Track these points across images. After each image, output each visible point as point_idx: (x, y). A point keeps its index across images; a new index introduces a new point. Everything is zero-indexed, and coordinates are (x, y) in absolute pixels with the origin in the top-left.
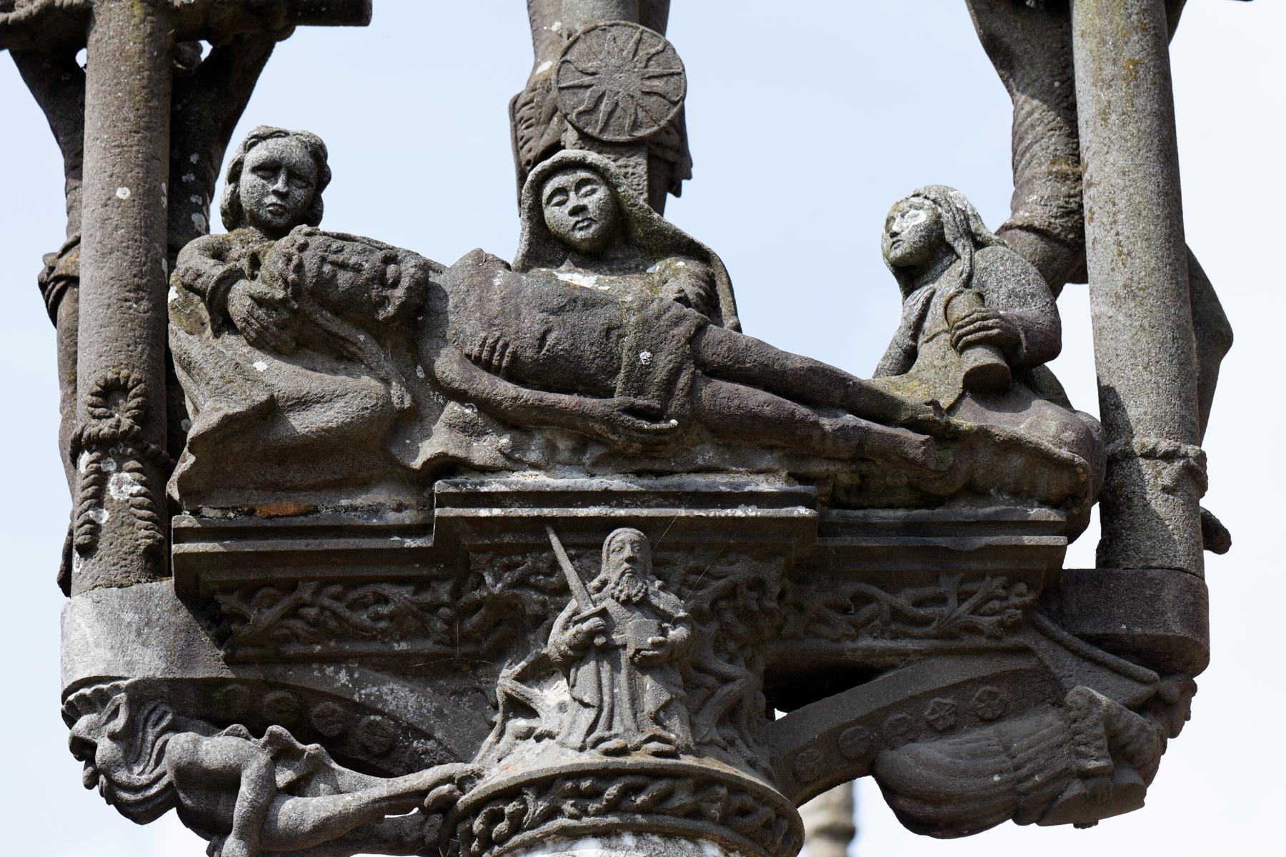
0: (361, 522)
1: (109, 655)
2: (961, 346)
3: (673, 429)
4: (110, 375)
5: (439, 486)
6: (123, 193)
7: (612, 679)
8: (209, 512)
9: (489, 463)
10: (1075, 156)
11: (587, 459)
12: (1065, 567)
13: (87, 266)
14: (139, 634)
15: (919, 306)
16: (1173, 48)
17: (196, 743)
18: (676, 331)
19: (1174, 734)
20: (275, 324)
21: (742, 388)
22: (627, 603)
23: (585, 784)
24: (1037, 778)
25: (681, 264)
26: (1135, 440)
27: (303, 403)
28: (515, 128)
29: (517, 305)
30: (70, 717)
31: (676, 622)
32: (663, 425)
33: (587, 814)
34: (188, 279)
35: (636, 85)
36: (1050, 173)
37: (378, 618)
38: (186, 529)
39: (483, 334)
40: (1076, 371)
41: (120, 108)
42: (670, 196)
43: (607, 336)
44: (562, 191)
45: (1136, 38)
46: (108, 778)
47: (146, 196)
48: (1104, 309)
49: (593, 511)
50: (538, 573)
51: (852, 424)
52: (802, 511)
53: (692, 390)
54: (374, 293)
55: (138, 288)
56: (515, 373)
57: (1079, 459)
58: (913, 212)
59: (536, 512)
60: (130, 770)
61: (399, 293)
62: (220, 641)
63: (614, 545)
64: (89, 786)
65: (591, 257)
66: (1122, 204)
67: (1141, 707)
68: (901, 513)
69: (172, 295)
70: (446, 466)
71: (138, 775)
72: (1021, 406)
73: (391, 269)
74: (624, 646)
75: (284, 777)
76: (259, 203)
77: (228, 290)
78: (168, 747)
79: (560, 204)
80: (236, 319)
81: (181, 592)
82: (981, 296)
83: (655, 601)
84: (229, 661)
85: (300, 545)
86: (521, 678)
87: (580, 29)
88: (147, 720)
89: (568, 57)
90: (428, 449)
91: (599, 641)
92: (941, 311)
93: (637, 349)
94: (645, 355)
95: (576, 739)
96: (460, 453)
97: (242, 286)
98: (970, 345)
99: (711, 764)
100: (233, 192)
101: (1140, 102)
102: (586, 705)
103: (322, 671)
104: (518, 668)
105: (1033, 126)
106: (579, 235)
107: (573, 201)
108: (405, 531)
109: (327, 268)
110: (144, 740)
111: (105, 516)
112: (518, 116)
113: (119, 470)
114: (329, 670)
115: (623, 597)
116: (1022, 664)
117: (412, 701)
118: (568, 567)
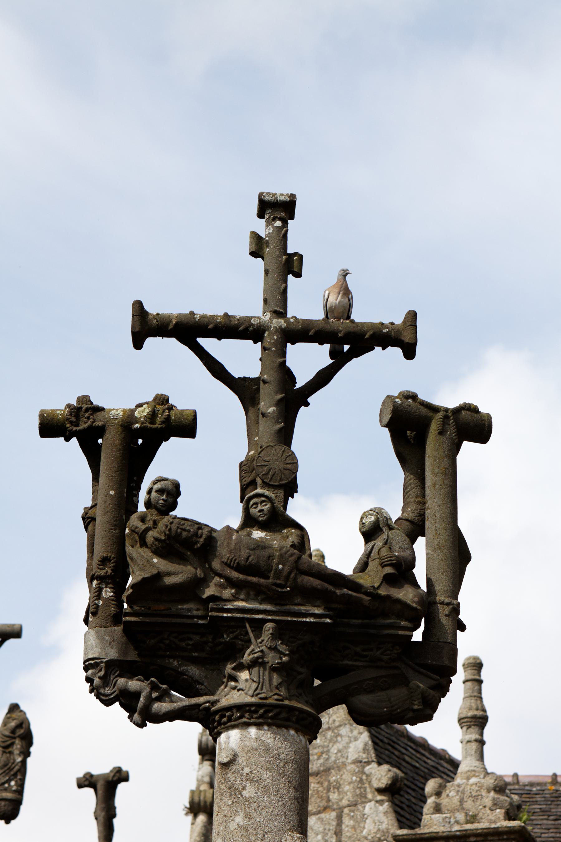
0: (185, 614)
1: (100, 650)
2: (383, 566)
3: (288, 591)
4: (105, 555)
5: (211, 605)
6: (112, 493)
7: (263, 673)
8: (136, 608)
9: (228, 598)
10: (424, 496)
11: (259, 598)
12: (412, 640)
13: (98, 513)
14: (110, 644)
15: (370, 548)
16: (458, 458)
17: (127, 682)
18: (291, 559)
19: (444, 696)
20: (161, 547)
21: (311, 578)
22: (270, 648)
23: (253, 708)
24: (398, 710)
25: (293, 531)
26: (437, 598)
27: (169, 574)
28: (240, 473)
29: (240, 546)
30: (86, 669)
31: (285, 655)
32: (285, 590)
33: (253, 718)
34: (133, 528)
35: (282, 466)
36: (415, 501)
37: (188, 645)
38: (128, 613)
39: (228, 555)
40: (420, 572)
41: (113, 463)
42: (290, 498)
43: (269, 560)
44: (256, 504)
45: (446, 460)
46: (97, 691)
47: (119, 493)
48: (430, 551)
49: (260, 616)
50: (241, 635)
51: (346, 593)
52: (328, 620)
53: (295, 579)
54: (194, 539)
55: (115, 525)
56: (238, 568)
57: (419, 607)
58: (370, 516)
59: (242, 616)
60: (105, 689)
61: (202, 540)
62: (136, 649)
63: (267, 629)
64: (91, 692)
65: (263, 526)
66: (438, 516)
67: (433, 688)
68: (360, 621)
69: (127, 531)
70: (213, 598)
71: (107, 691)
72: (401, 586)
73: (200, 531)
74: (268, 663)
75: (155, 695)
76: (157, 503)
77: (146, 534)
78: (118, 683)
79: (255, 508)
80: (148, 544)
81: (124, 631)
82: (390, 548)
83: (279, 647)
84: (139, 655)
85: (165, 620)
86: (233, 669)
87: (265, 445)
88: (111, 673)
89: (260, 455)
90: (209, 592)
91: (260, 660)
92: (377, 551)
93: (279, 564)
94: (280, 566)
95: (251, 692)
96: (217, 594)
97: (150, 533)
98: (386, 566)
99: (295, 704)
100: (149, 498)
101: (446, 482)
102: (255, 682)
103: (169, 660)
104: (233, 665)
105: (410, 484)
106: (261, 519)
107: (260, 508)
108: (199, 618)
109: (179, 530)
110: (110, 679)
111: (101, 603)
112: (242, 469)
113: (106, 587)
114: (171, 660)
115: (268, 646)
117: (198, 672)
118: (251, 635)
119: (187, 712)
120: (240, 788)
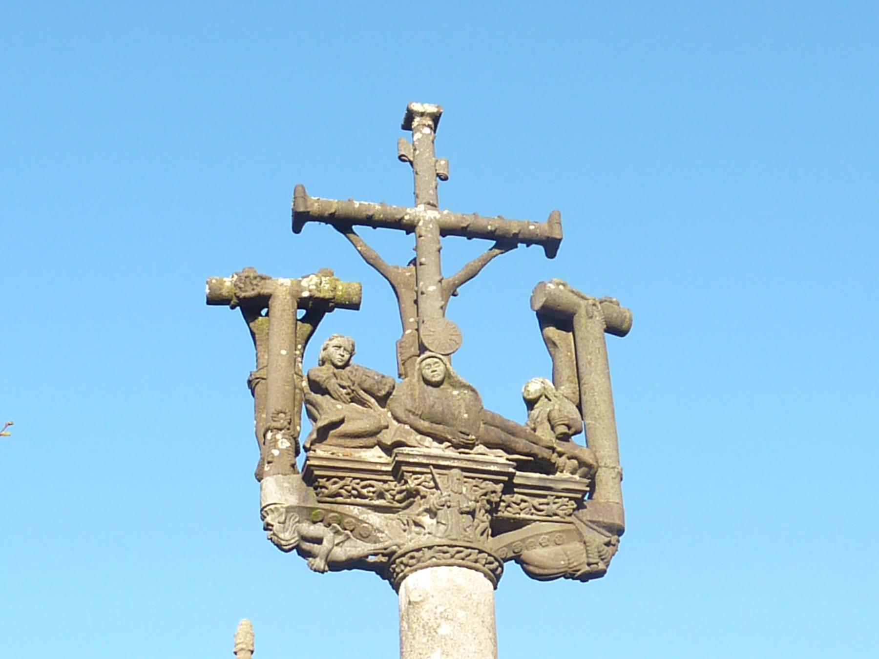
44: (429, 365)
116: (570, 526)
117: (378, 520)
119: (370, 557)
120: (435, 626)
